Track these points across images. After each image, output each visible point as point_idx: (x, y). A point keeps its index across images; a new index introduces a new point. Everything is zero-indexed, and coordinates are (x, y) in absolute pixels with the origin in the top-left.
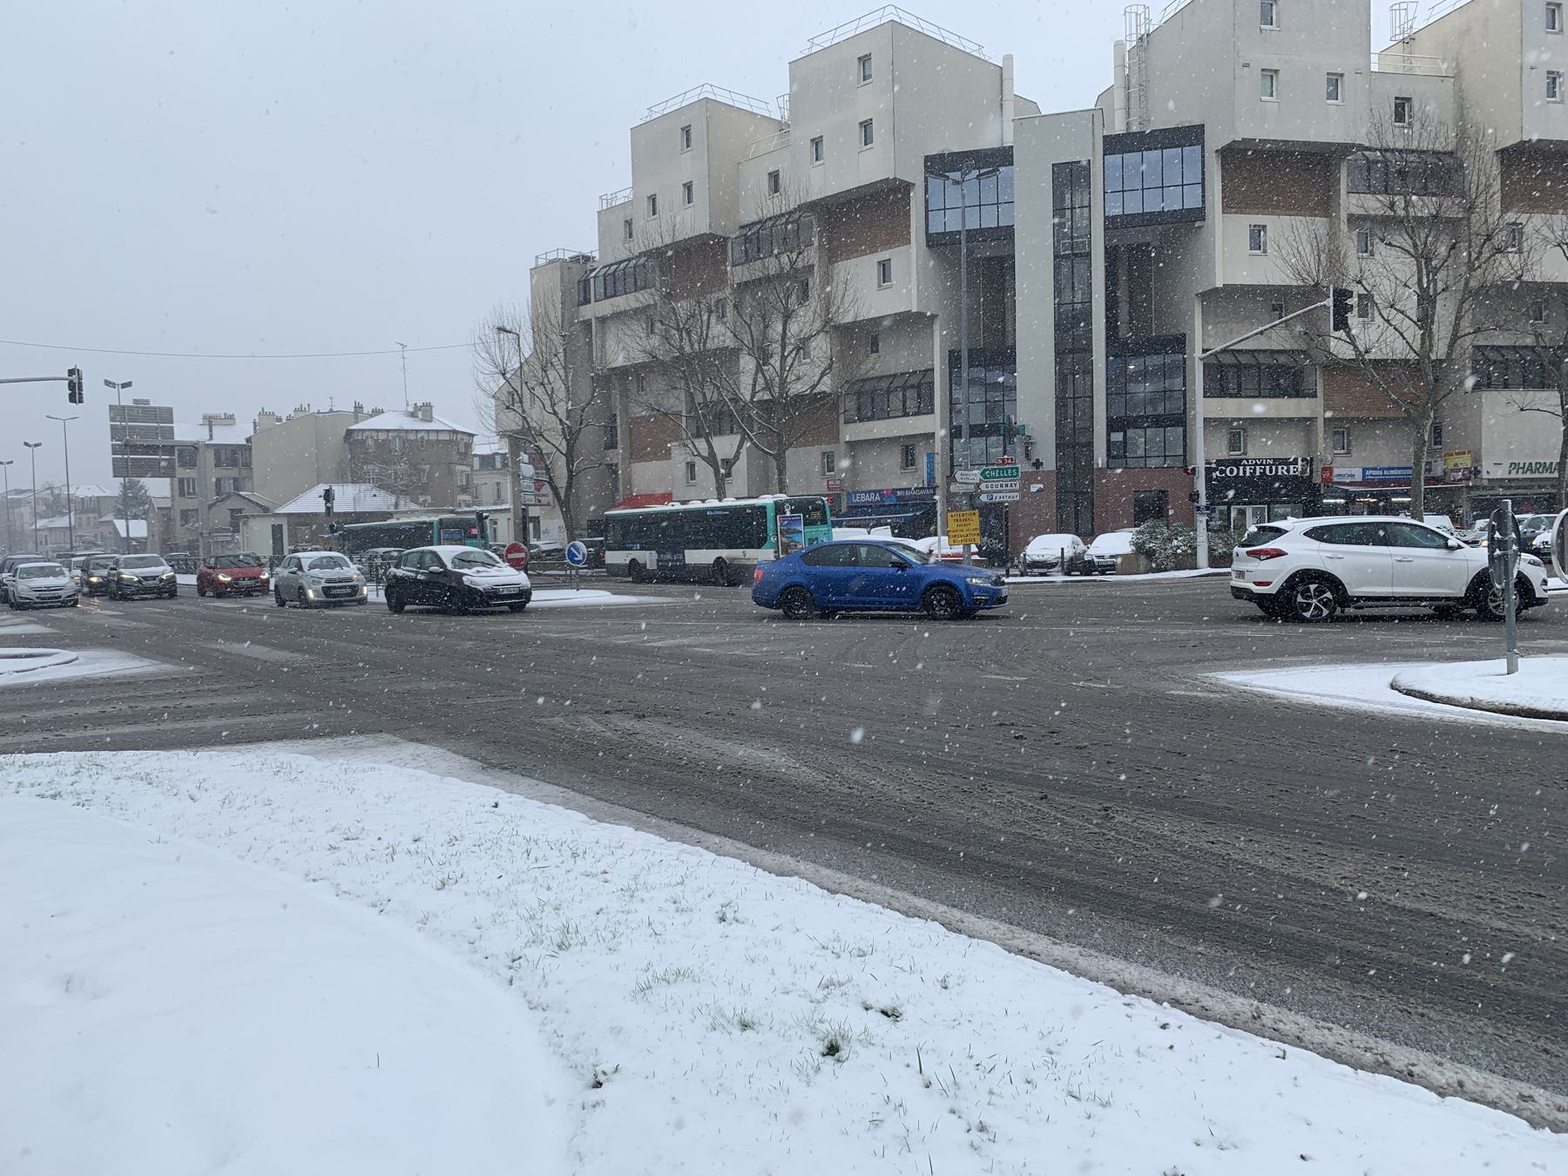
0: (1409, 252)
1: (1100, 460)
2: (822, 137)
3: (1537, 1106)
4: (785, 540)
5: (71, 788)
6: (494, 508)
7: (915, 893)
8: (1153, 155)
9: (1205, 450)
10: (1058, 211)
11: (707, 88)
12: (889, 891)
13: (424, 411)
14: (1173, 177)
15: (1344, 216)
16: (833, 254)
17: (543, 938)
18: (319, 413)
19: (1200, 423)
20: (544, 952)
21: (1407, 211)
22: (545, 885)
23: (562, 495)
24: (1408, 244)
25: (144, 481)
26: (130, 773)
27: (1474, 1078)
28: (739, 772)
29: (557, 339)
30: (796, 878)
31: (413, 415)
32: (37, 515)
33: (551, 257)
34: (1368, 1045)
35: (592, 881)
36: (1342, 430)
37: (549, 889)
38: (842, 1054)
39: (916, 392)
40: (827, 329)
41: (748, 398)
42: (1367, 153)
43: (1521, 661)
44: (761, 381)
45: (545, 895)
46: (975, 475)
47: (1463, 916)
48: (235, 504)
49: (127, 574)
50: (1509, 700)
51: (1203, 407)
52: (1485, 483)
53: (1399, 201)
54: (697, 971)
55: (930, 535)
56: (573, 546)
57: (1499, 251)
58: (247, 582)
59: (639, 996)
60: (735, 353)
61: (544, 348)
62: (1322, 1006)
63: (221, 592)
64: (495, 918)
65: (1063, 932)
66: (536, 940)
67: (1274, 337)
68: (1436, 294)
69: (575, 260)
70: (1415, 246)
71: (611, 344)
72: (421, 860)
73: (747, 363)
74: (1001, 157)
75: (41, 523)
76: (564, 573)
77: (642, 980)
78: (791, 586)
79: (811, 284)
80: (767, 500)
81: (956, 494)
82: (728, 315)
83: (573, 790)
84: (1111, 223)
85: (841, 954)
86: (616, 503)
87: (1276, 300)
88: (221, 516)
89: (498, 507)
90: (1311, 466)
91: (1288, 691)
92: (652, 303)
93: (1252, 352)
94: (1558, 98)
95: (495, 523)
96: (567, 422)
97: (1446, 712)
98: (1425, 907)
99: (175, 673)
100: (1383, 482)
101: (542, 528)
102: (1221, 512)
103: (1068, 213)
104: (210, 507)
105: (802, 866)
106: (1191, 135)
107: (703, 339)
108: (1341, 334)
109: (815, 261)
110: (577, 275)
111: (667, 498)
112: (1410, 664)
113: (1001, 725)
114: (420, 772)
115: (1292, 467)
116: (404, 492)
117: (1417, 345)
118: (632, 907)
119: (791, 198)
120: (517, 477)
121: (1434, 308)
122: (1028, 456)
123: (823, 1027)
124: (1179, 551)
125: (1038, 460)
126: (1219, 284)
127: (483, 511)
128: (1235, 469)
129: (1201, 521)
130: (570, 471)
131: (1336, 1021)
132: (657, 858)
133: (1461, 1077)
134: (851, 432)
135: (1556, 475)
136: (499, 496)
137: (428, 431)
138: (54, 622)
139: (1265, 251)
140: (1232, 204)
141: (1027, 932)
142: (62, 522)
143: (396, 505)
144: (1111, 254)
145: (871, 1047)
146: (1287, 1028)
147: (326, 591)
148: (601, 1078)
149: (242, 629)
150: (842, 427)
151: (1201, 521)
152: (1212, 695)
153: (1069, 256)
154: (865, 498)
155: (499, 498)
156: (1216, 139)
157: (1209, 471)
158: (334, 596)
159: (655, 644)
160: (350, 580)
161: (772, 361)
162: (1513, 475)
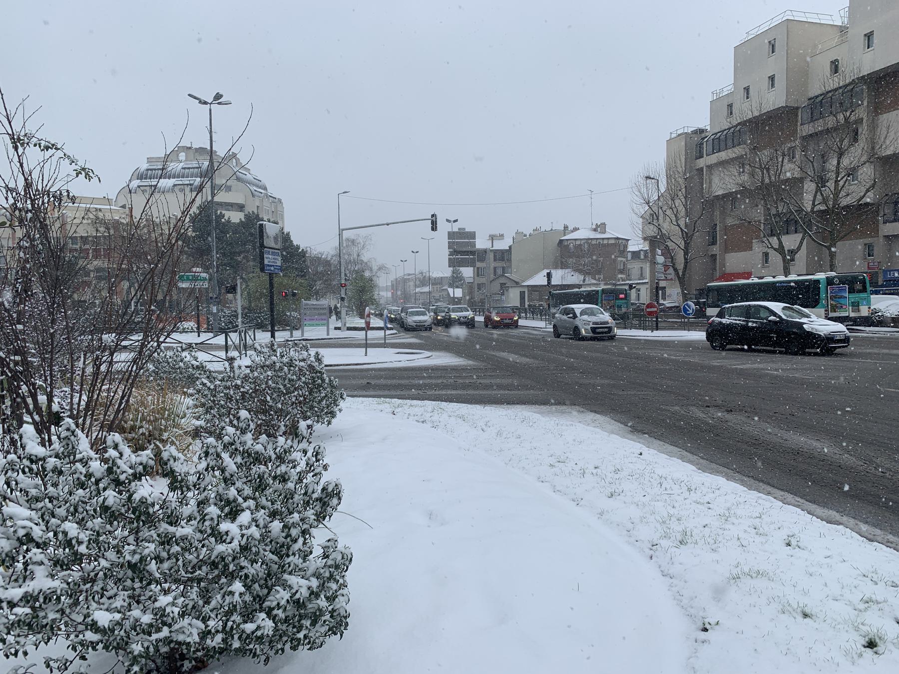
2: (873, 31)
4: (834, 303)
5: (430, 419)
6: (639, 282)
11: (788, 13)
13: (600, 227)
17: (671, 535)
18: (545, 231)
20: (671, 544)
22: (671, 505)
23: (681, 274)
25: (462, 269)
26: (455, 414)
28: (797, 453)
29: (681, 181)
30: (841, 527)
31: (595, 230)
32: (416, 286)
33: (679, 132)
35: (699, 506)
37: (673, 507)
38: (880, 648)
40: (871, 160)
41: (809, 209)
44: (819, 197)
45: (672, 511)
48: (502, 280)
49: (454, 315)
54: (771, 574)
56: (687, 305)
58: (507, 321)
59: (732, 581)
60: (801, 180)
61: (673, 187)
63: (496, 326)
64: (642, 519)
66: (666, 536)
71: (716, 180)
72: (600, 479)
73: (809, 187)
75: (418, 290)
76: (680, 320)
77: (735, 572)
79: (860, 130)
80: (821, 276)
82: (797, 156)
83: (686, 451)
85: (879, 582)
86: (715, 278)
88: (496, 287)
89: (641, 281)
92: (744, 153)
95: (639, 291)
96: (686, 230)
99: (474, 365)
101: (667, 294)
104: (491, 282)
105: (845, 519)
107: (778, 173)
109: (864, 115)
110: (696, 138)
111: (748, 275)
114: (597, 430)
116: (589, 274)
118: (727, 526)
119: (849, 74)
120: (654, 263)
123: (865, 629)
127: (633, 284)
130: (686, 259)
132: (742, 500)
136: (642, 274)
137: (603, 239)
138: (420, 338)
142: (426, 289)
143: (584, 280)
147: (594, 330)
148: (708, 626)
149: (505, 346)
150: (881, 226)
155: (642, 276)
158: (599, 333)
159: (739, 367)
160: (607, 323)
161: (828, 184)
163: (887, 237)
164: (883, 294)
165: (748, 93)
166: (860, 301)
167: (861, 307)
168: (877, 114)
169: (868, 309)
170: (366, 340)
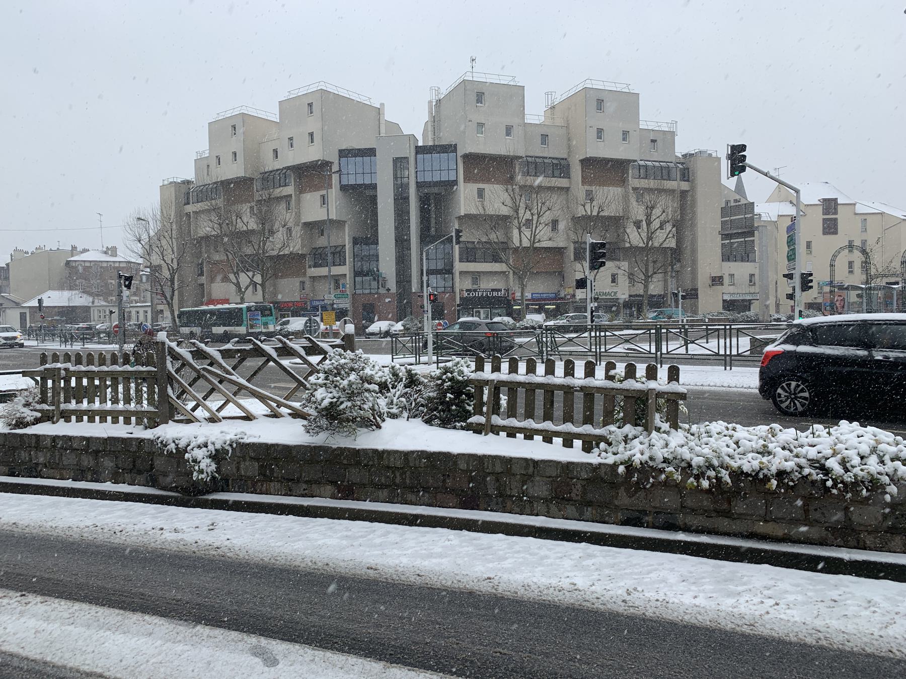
11: (322, 83)
13: (113, 251)
14: (436, 166)
16: (301, 190)
31: (106, 253)
39: (338, 255)
51: (459, 266)
69: (184, 182)
84: (419, 185)
106: (450, 149)
110: (184, 189)
111: (227, 301)
116: (98, 295)
137: (114, 262)
140: (467, 179)
143: (93, 302)
153: (401, 200)
156: (461, 151)
165: (235, 156)
168: (301, 193)
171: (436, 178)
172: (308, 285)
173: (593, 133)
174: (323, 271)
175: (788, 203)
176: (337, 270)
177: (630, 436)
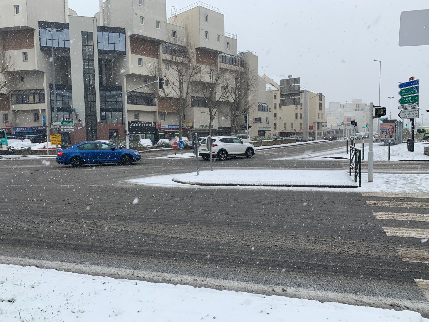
0: (176, 71)
1: (99, 120)
3: (198, 281)
7: (29, 258)
8: (111, 34)
9: (128, 119)
10: (84, 45)
12: (20, 259)
15: (161, 59)
19: (126, 111)
21: (176, 60)
24: (176, 68)
27: (184, 278)
34: (161, 275)
36: (163, 115)
40: (3, 72)
42: (167, 44)
43: (200, 172)
46: (59, 123)
47: (185, 237)
50: (197, 182)
51: (127, 107)
52: (195, 130)
53: (174, 58)
55: (44, 142)
57: (196, 73)
62: (150, 267)
65: (78, 261)
67: (145, 89)
68: (183, 82)
70: (178, 69)
74: (65, 26)
78: (75, 157)
81: (53, 129)
84: (100, 52)
87: (146, 79)
90: (156, 124)
91: (148, 183)
93: (140, 93)
94: (207, 38)
97: (183, 186)
98: (177, 236)
100: (173, 129)
102: (133, 136)
103: (87, 46)
106: (122, 31)
108: (161, 90)
112: (177, 174)
113: (64, 200)
115: (151, 124)
117: (179, 94)
121: (182, 85)
122: (76, 118)
124: (121, 147)
125: (80, 119)
126: (131, 73)
128: (136, 124)
129: (127, 138)
131: (153, 271)
133: (182, 278)
134: (14, 107)
135: (209, 128)
139: (142, 66)
141: (67, 263)
144: (100, 60)
145: (2, 314)
146: (141, 275)
151: (127, 138)
152: (128, 186)
154: (20, 130)
157: (129, 124)
162: (200, 128)
163: (14, 111)
164: (14, 139)
166: (2, 143)
167: (3, 146)
169: (6, 147)
170: (210, 126)
171: (112, 49)
172: (11, 117)
173: (203, 34)
174: (25, 107)
175: (270, 85)
176: (39, 107)
177: (46, 147)
